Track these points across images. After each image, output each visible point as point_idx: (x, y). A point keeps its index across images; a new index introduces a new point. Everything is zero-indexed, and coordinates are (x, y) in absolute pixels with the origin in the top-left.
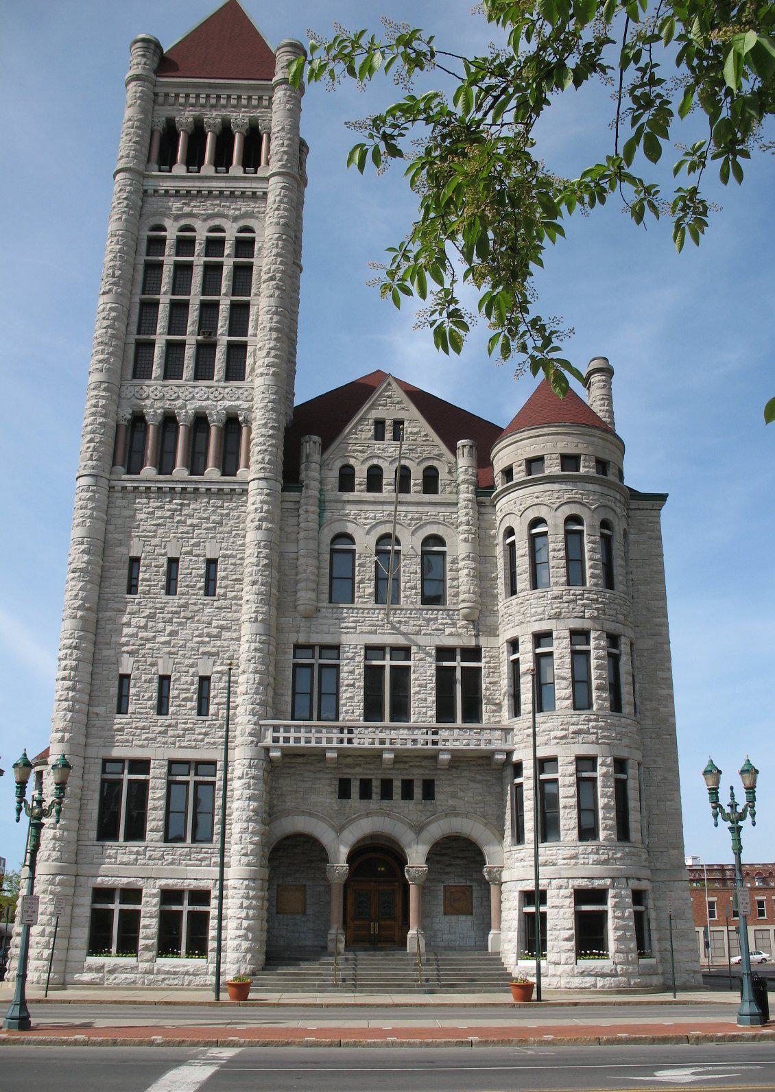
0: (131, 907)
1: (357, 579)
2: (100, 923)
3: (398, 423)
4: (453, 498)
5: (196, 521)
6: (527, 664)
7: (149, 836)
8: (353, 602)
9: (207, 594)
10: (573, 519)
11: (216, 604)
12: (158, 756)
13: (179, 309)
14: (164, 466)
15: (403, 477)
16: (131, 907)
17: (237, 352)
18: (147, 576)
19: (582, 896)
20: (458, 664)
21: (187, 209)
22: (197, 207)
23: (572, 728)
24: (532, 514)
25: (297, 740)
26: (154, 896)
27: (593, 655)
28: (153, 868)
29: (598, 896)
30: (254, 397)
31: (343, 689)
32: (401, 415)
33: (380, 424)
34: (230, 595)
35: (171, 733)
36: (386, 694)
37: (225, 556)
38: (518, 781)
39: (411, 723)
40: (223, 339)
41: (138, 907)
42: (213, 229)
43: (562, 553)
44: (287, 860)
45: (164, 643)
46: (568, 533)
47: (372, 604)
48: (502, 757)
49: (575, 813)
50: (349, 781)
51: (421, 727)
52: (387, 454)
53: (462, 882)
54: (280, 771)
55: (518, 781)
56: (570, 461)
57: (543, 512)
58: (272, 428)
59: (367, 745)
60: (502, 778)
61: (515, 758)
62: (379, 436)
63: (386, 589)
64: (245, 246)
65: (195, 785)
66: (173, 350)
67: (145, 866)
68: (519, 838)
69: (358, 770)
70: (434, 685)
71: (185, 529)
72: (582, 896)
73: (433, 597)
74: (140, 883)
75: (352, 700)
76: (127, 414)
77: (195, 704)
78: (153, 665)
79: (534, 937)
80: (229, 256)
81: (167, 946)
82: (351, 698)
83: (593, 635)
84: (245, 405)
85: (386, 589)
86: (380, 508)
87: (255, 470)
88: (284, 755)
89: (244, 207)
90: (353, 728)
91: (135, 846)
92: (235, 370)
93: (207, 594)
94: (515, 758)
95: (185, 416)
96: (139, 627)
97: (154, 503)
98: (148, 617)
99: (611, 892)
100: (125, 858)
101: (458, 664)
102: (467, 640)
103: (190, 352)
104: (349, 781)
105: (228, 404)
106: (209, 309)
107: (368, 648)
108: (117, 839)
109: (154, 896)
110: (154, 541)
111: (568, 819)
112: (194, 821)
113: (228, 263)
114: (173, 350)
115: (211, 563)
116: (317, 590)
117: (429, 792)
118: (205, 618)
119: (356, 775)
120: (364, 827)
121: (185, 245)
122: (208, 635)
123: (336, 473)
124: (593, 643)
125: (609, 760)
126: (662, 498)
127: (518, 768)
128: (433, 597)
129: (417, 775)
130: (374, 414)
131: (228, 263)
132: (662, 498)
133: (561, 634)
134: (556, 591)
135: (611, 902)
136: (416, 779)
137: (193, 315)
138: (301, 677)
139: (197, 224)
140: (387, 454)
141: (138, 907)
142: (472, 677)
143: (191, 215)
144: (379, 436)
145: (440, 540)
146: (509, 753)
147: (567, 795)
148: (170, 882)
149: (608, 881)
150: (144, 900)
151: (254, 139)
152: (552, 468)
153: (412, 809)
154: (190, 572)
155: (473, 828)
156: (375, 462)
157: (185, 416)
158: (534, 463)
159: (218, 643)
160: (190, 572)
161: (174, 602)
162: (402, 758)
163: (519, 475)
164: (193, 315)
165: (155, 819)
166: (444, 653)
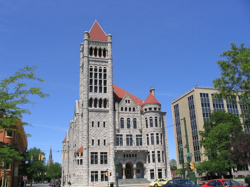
0: (97, 174)
1: (124, 125)
2: (92, 177)
3: (129, 101)
4: (137, 112)
5: (102, 116)
6: (150, 138)
7: (98, 163)
8: (124, 128)
9: (104, 127)
10: (156, 117)
11: (106, 129)
12: (99, 152)
13: (96, 81)
14: (95, 106)
15: (130, 109)
16: (97, 174)
17: (105, 89)
18: (95, 124)
19: (151, 170)
20: (129, 137)
21: (95, 63)
22: (98, 63)
23: (157, 147)
24: (150, 116)
25: (129, 149)
26: (100, 172)
27: (159, 137)
28: (99, 168)
29: (161, 170)
30: (109, 96)
31: (123, 141)
32: (129, 99)
33: (126, 101)
34: (107, 127)
35: (100, 148)
36: (129, 141)
37: (106, 121)
38: (149, 154)
39: (143, 146)
40: (103, 86)
41: (98, 174)
42: (100, 67)
43: (155, 122)
44: (118, 167)
45: (98, 135)
46: (155, 119)
47: (127, 128)
48: (147, 151)
49: (157, 159)
50: (125, 155)
51: (134, 148)
52: (128, 105)
53: (139, 168)
54: (117, 153)
55: (149, 154)
56: (155, 109)
57: (152, 116)
58: (112, 102)
59: (127, 150)
60: (225, 150)
61: (148, 151)
62: (126, 102)
63: (129, 126)
64: (105, 71)
65: (104, 155)
66: (96, 88)
67: (99, 168)
68: (149, 162)
69: (126, 153)
70: (136, 140)
71: (100, 117)
72: (159, 170)
73: (135, 127)
74: (98, 170)
75: (124, 142)
76: (90, 98)
77: (103, 144)
78: (97, 138)
79: (152, 175)
80: (103, 72)
81: (102, 180)
82: (124, 143)
83: (159, 134)
84: (107, 97)
85: (129, 126)
86: (127, 114)
87: (110, 107)
88: (117, 151)
89: (105, 64)
90: (124, 147)
91: (96, 165)
92: (105, 91)
93: (104, 127)
94: (148, 151)
95: (99, 98)
96: (95, 132)
97: (95, 113)
98: (96, 131)
99: (162, 169)
100: (95, 167)
101: (129, 137)
102: (140, 134)
103: (98, 88)
104: (125, 155)
105: (105, 97)
106: (100, 81)
107: (136, 135)
108: (93, 164)
109: (100, 172)
110: (96, 119)
111: (157, 160)
112: (104, 161)
113: (103, 74)
114: (96, 88)
115: (104, 123)
116: (119, 127)
117: (136, 156)
118: (104, 131)
119: (126, 154)
120: (127, 161)
121: (96, 70)
122: (105, 133)
123: (121, 108)
124: (159, 135)
125: (162, 151)
126: (166, 113)
127: (149, 153)
128: (135, 127)
129: (134, 154)
130: (125, 99)
131: (103, 74)
132: (166, 113)
133: (155, 134)
134: (154, 128)
135: (162, 171)
136: (134, 155)
137: (98, 82)
138: (118, 140)
139: (97, 66)
140: (128, 105)
141: (98, 174)
142: (131, 139)
143: (96, 65)
144: (126, 102)
145: (136, 119)
146: (147, 150)
147: (156, 156)
148: (102, 170)
149: (162, 168)
150: (98, 173)
151: (105, 51)
152: (153, 110)
153: (134, 158)
154: (101, 124)
155: (142, 161)
156: (126, 107)
157: (99, 98)
158: (150, 109)
159: (106, 135)
160: (101, 124)
161: (99, 128)
162: (134, 151)
163: (148, 110)
164: (98, 82)
165: (99, 161)
166: (137, 136)
